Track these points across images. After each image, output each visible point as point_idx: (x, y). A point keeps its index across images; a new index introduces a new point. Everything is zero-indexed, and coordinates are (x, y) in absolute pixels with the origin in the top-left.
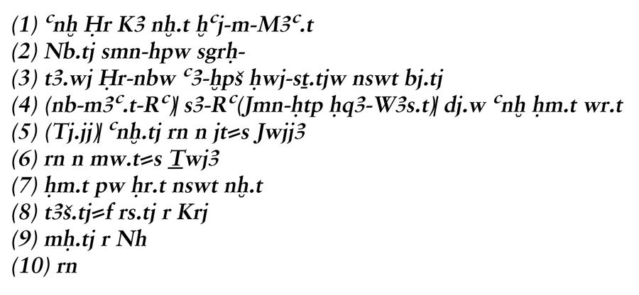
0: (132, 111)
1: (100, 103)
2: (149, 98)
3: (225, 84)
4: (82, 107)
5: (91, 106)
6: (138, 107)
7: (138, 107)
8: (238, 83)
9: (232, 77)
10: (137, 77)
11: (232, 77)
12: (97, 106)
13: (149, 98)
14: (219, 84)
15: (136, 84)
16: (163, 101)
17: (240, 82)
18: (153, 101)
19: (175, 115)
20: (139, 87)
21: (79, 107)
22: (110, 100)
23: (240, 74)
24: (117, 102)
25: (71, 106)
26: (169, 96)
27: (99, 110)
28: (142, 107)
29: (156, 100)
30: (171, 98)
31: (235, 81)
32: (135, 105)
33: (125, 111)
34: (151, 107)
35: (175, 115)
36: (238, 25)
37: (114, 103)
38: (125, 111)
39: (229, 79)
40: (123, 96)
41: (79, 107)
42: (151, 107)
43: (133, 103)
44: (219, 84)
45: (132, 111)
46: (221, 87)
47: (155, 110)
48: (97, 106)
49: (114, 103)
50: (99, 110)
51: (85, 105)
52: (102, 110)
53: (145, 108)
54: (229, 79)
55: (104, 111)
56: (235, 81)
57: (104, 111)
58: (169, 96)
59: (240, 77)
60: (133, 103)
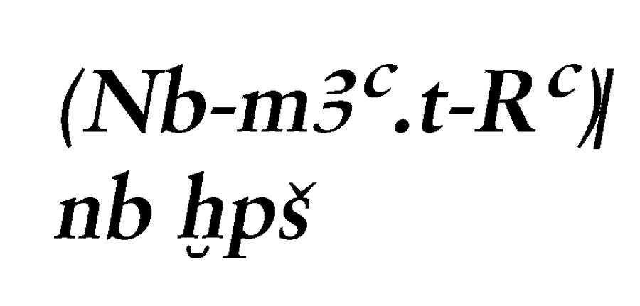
0: (429, 126)
1: (301, 98)
2: (497, 77)
3: (239, 234)
4: (231, 111)
5: (264, 106)
6: (455, 111)
7: (455, 111)
8: (291, 229)
9: (267, 205)
10: (252, 99)
11: (267, 205)
12: (289, 106)
13: (497, 77)
14: (214, 231)
15: (248, 125)
16: (554, 90)
17: (301, 224)
18: (510, 87)
19: (597, 145)
20: (260, 139)
21: (216, 111)
22: (339, 83)
23: (300, 195)
24: (370, 91)
25: (185, 109)
26: (577, 68)
27: (298, 125)
28: (469, 111)
29: (526, 82)
30: (585, 79)
31: (280, 220)
32: (442, 106)
33: (402, 126)
34: (503, 115)
35: (597, 145)
36: (264, 106)
37: (356, 96)
38: (402, 126)
39: (255, 216)
40: (393, 68)
41: (216, 111)
42: (503, 115)
43: (433, 95)
44: (214, 231)
45: (429, 126)
46: (223, 245)
47: (521, 124)
48: (289, 106)
49: (356, 96)
50: (298, 125)
51: (241, 106)
52: (308, 123)
53: (479, 118)
54: (255, 216)
55: (317, 128)
56: (280, 220)
57: (317, 128)
58: (577, 68)
59: (298, 207)
60: (433, 95)
